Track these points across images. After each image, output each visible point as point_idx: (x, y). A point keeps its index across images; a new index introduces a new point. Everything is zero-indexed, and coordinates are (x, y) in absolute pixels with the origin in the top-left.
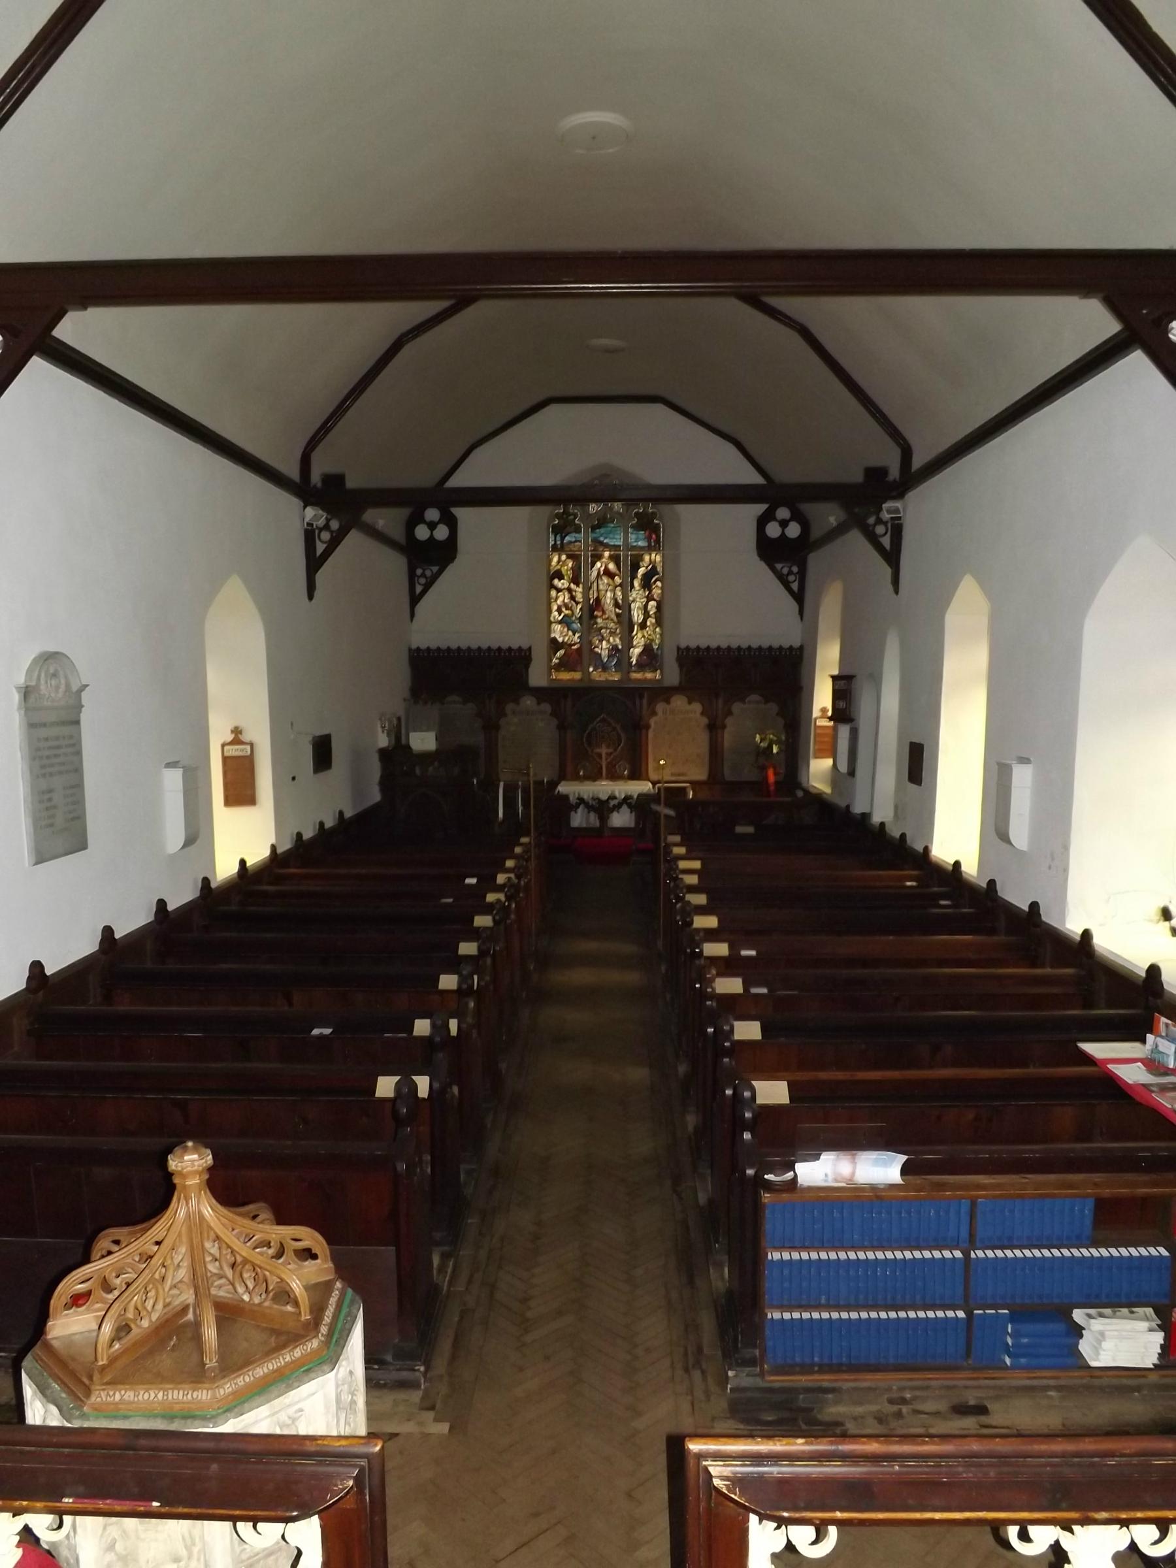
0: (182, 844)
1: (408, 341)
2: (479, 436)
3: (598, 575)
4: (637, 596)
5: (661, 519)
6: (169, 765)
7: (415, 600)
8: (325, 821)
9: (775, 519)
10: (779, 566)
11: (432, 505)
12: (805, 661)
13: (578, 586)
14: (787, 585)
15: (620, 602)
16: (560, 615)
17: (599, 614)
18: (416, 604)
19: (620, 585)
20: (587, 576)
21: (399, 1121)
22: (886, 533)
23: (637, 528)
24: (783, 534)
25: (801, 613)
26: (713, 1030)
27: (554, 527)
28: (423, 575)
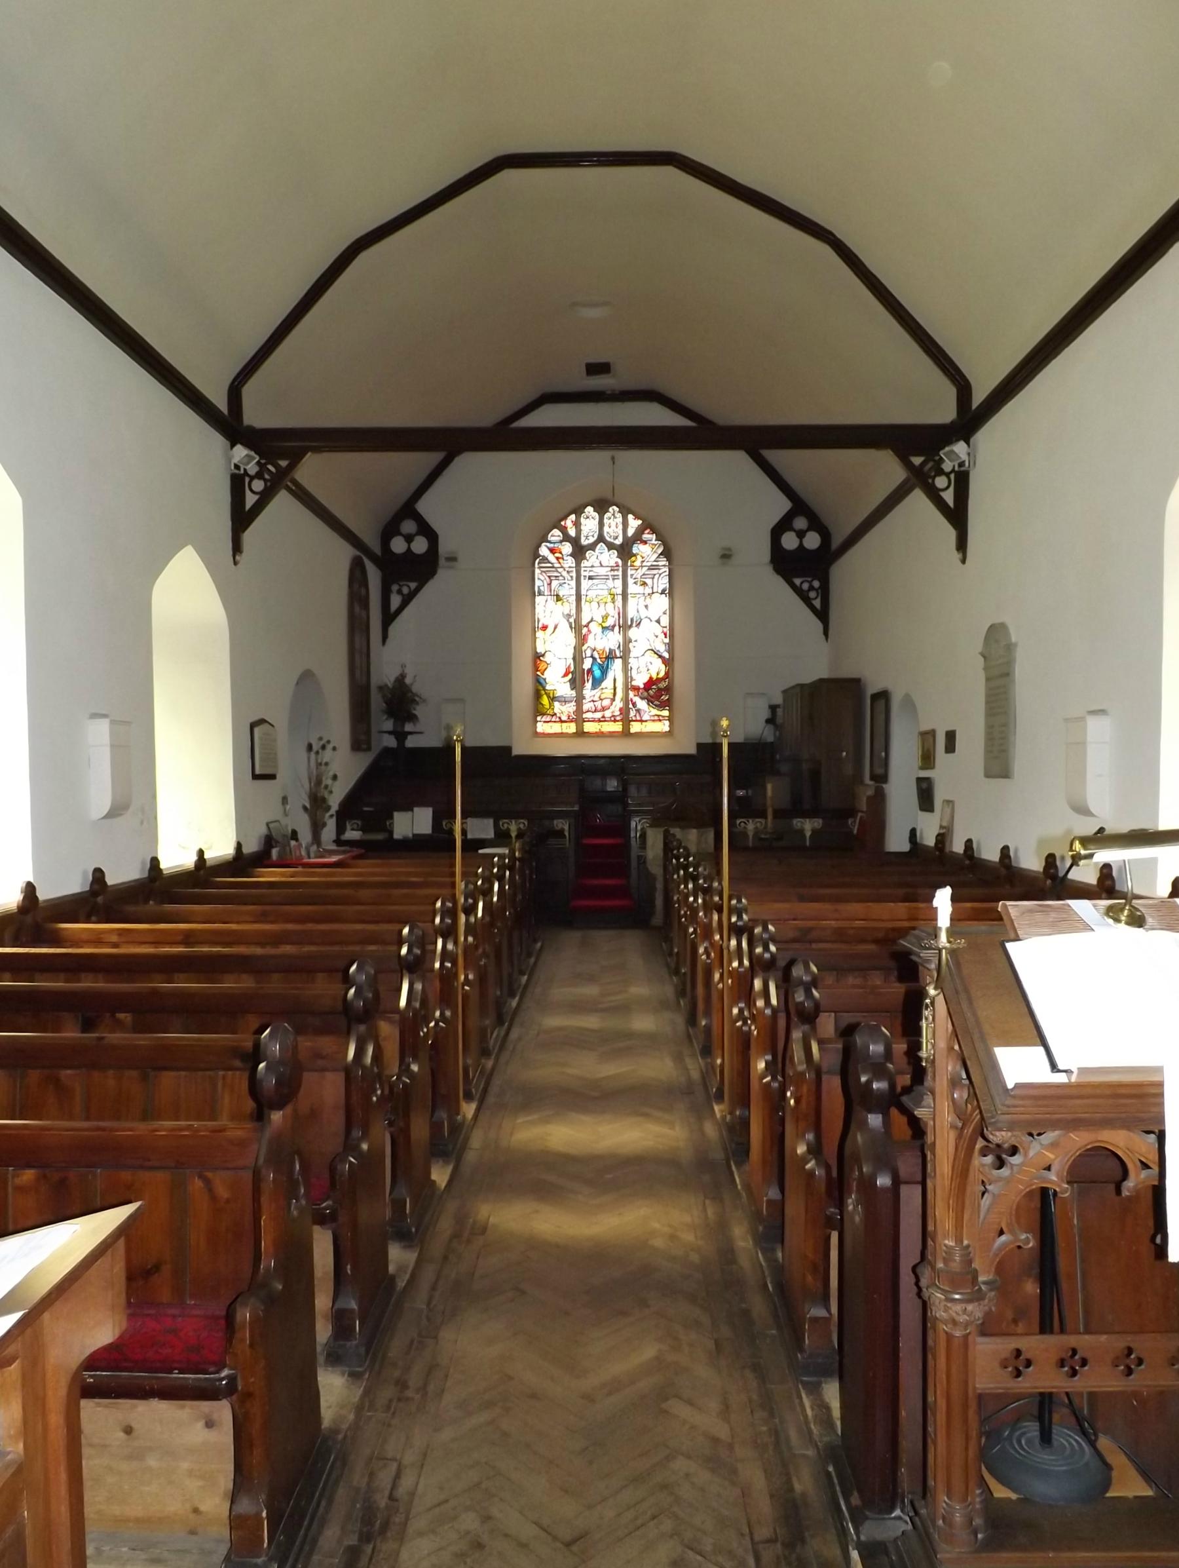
0: (105, 812)
6: (94, 716)
9: (792, 529)
10: (797, 581)
24: (801, 545)
25: (826, 633)
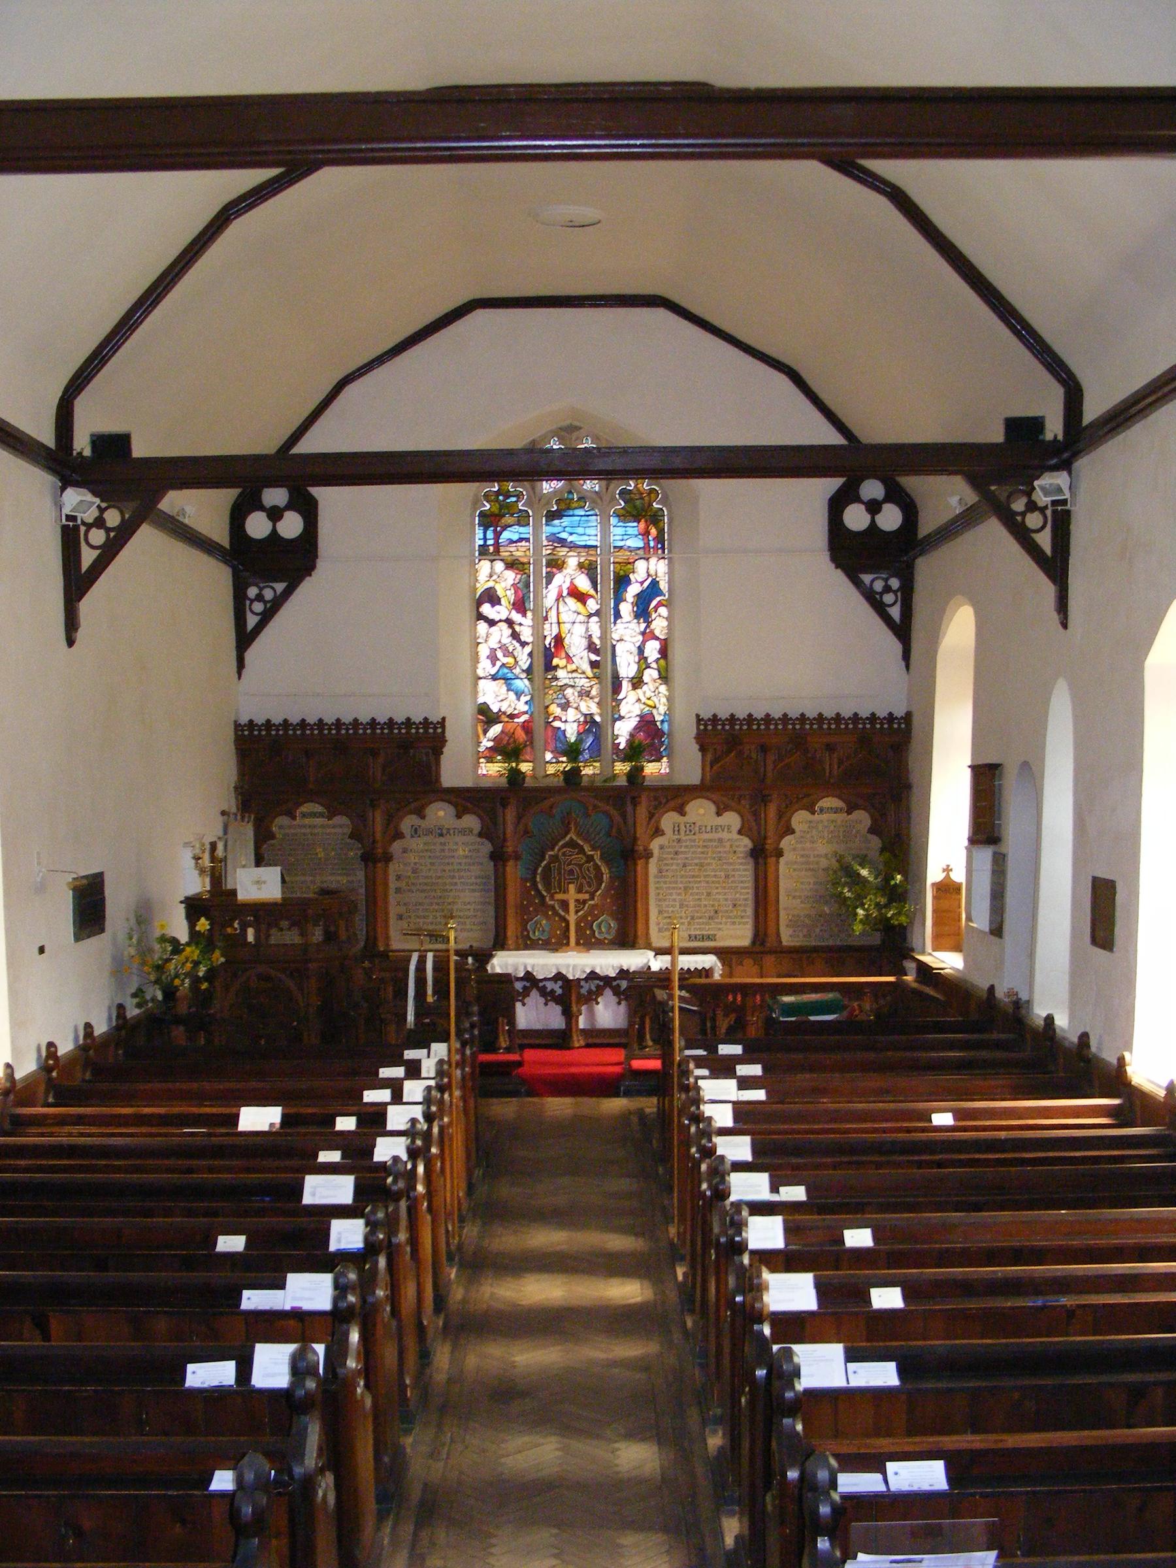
1: (238, 214)
2: (352, 367)
3: (560, 596)
4: (627, 631)
5: (664, 501)
7: (245, 639)
8: (93, 1023)
9: (858, 499)
10: (866, 578)
11: (275, 483)
12: (915, 745)
13: (524, 615)
14: (880, 609)
15: (597, 642)
16: (494, 665)
17: (562, 663)
18: (246, 650)
19: (597, 613)
20: (539, 598)
21: (240, 1529)
22: (1043, 527)
23: (624, 516)
25: (906, 656)
26: (765, 1371)
27: (482, 515)
28: (260, 598)
